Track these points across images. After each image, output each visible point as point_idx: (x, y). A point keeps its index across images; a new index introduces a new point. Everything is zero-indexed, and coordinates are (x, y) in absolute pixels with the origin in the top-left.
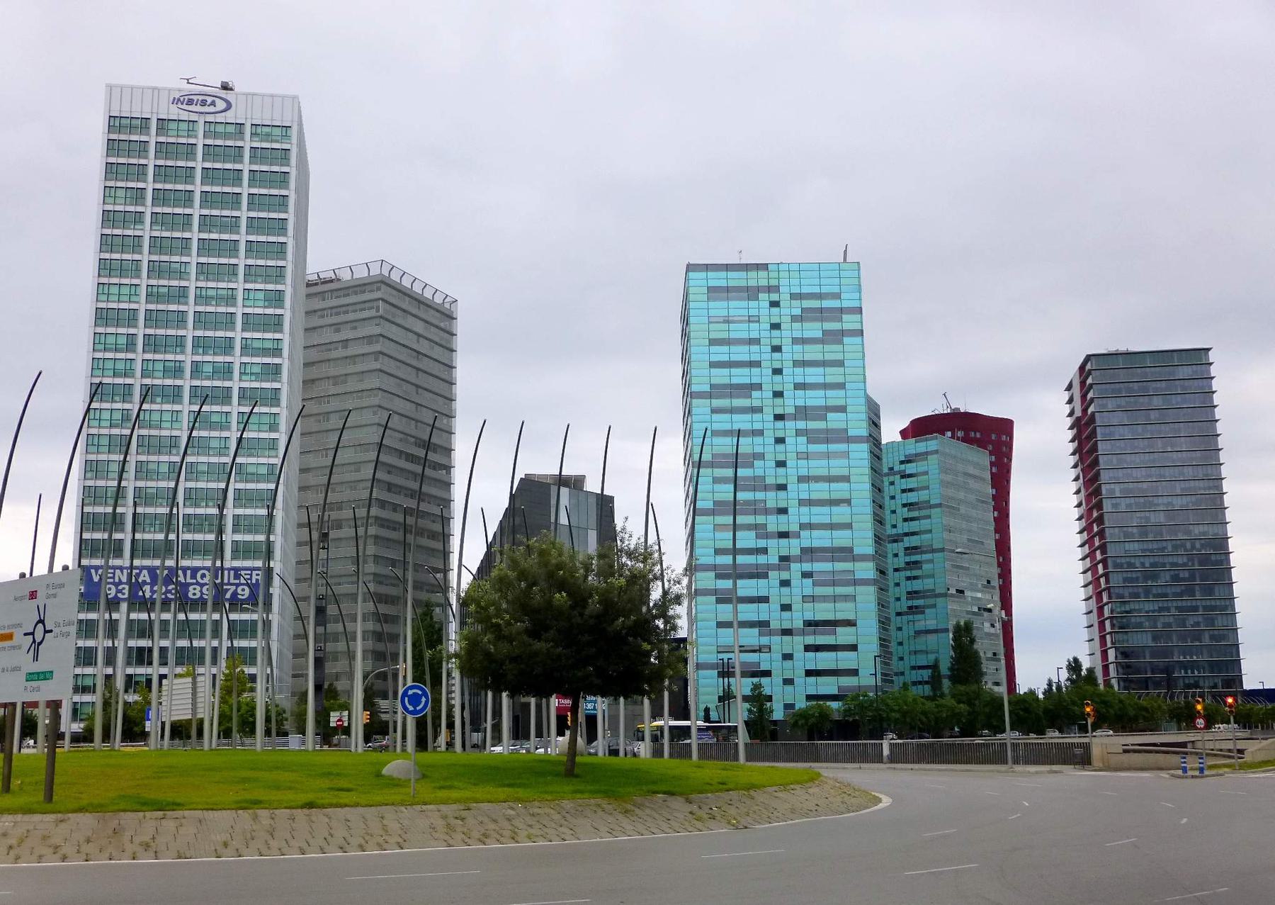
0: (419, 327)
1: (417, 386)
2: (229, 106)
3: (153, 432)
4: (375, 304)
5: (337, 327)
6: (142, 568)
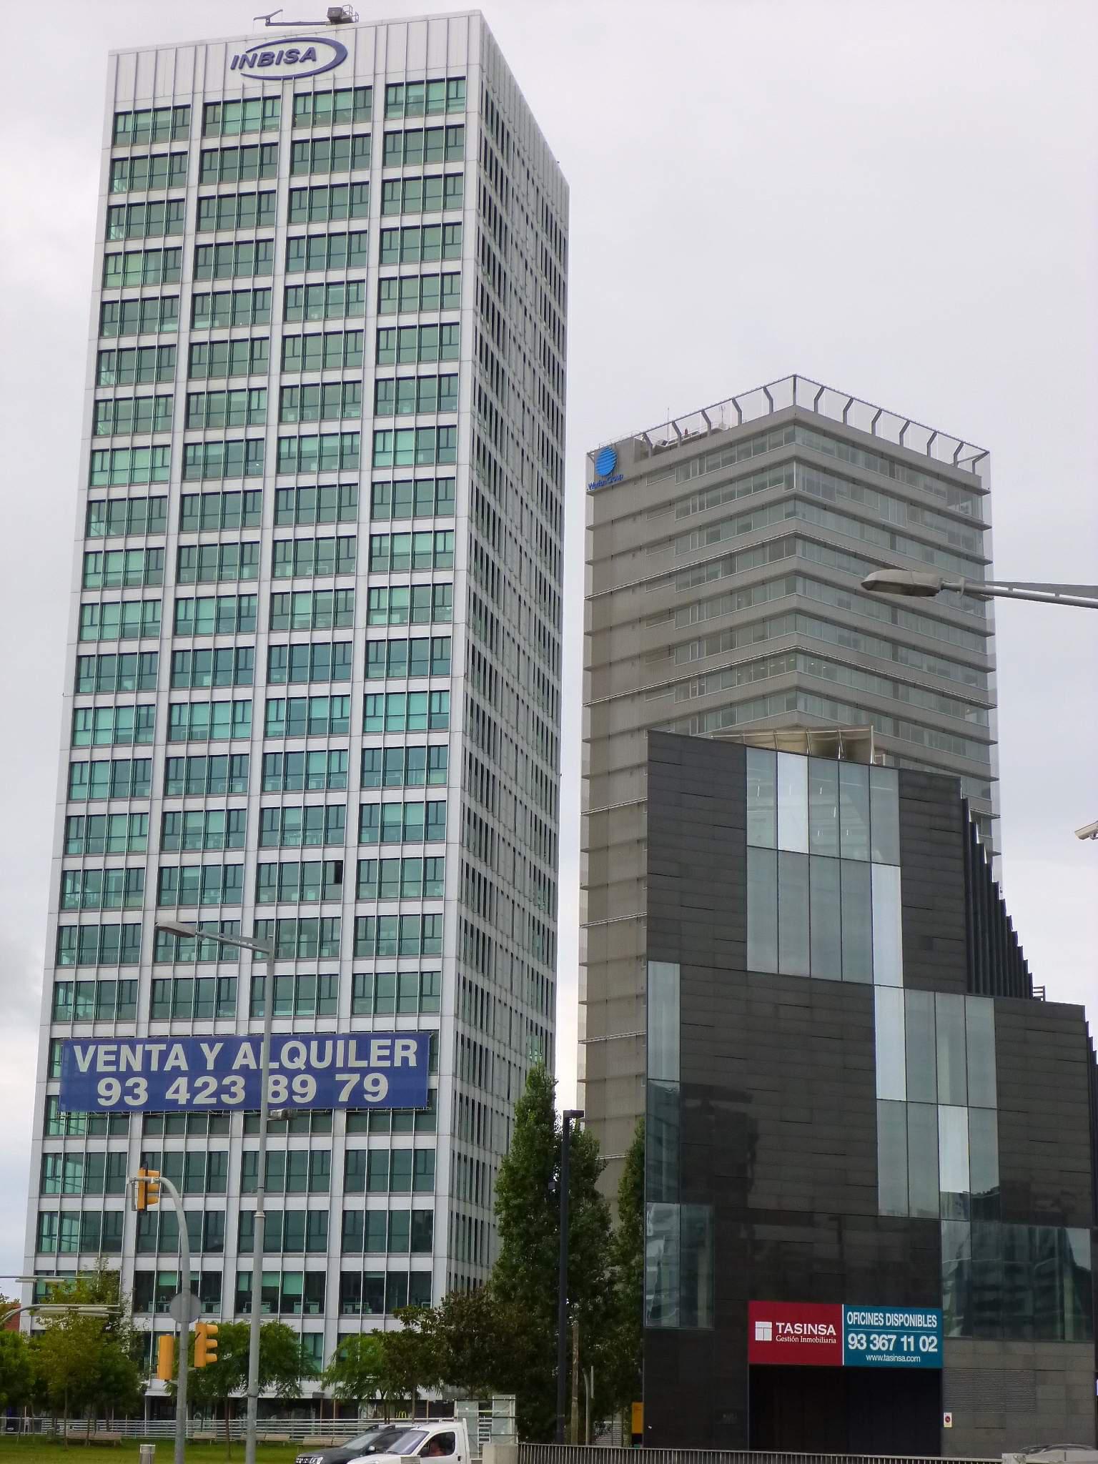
0: (894, 515)
1: (895, 643)
2: (341, 55)
3: (198, 749)
4: (783, 472)
5: (712, 530)
6: (170, 1040)
